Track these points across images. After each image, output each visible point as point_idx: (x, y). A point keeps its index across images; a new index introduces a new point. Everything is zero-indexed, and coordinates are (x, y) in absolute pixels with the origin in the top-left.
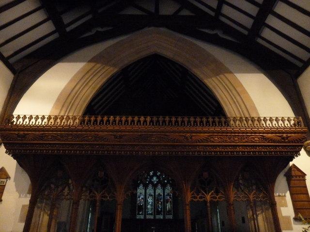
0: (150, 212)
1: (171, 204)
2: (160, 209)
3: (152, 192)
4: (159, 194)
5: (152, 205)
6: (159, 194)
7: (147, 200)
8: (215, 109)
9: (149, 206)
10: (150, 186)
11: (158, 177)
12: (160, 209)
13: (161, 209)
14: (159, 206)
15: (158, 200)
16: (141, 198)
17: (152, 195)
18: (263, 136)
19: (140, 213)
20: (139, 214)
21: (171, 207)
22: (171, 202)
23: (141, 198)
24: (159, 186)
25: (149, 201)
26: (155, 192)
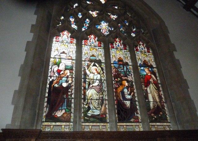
0: (97, 112)
1: (158, 89)
2: (128, 103)
3: (100, 54)
4: (120, 60)
5: (100, 90)
6: (120, 60)
7: (85, 74)
8: (125, 67)
9: (91, 93)
10: (92, 39)
11: (111, 23)
12: (128, 103)
13: (132, 101)
14: (123, 92)
15: (117, 76)
16: (62, 67)
17: (99, 62)
18: (38, 96)
19: (59, 114)
20: (51, 118)
21: (160, 97)
22: (156, 84)
23: (62, 67)
24: (118, 43)
25: (91, 76)
26: (133, 58)
